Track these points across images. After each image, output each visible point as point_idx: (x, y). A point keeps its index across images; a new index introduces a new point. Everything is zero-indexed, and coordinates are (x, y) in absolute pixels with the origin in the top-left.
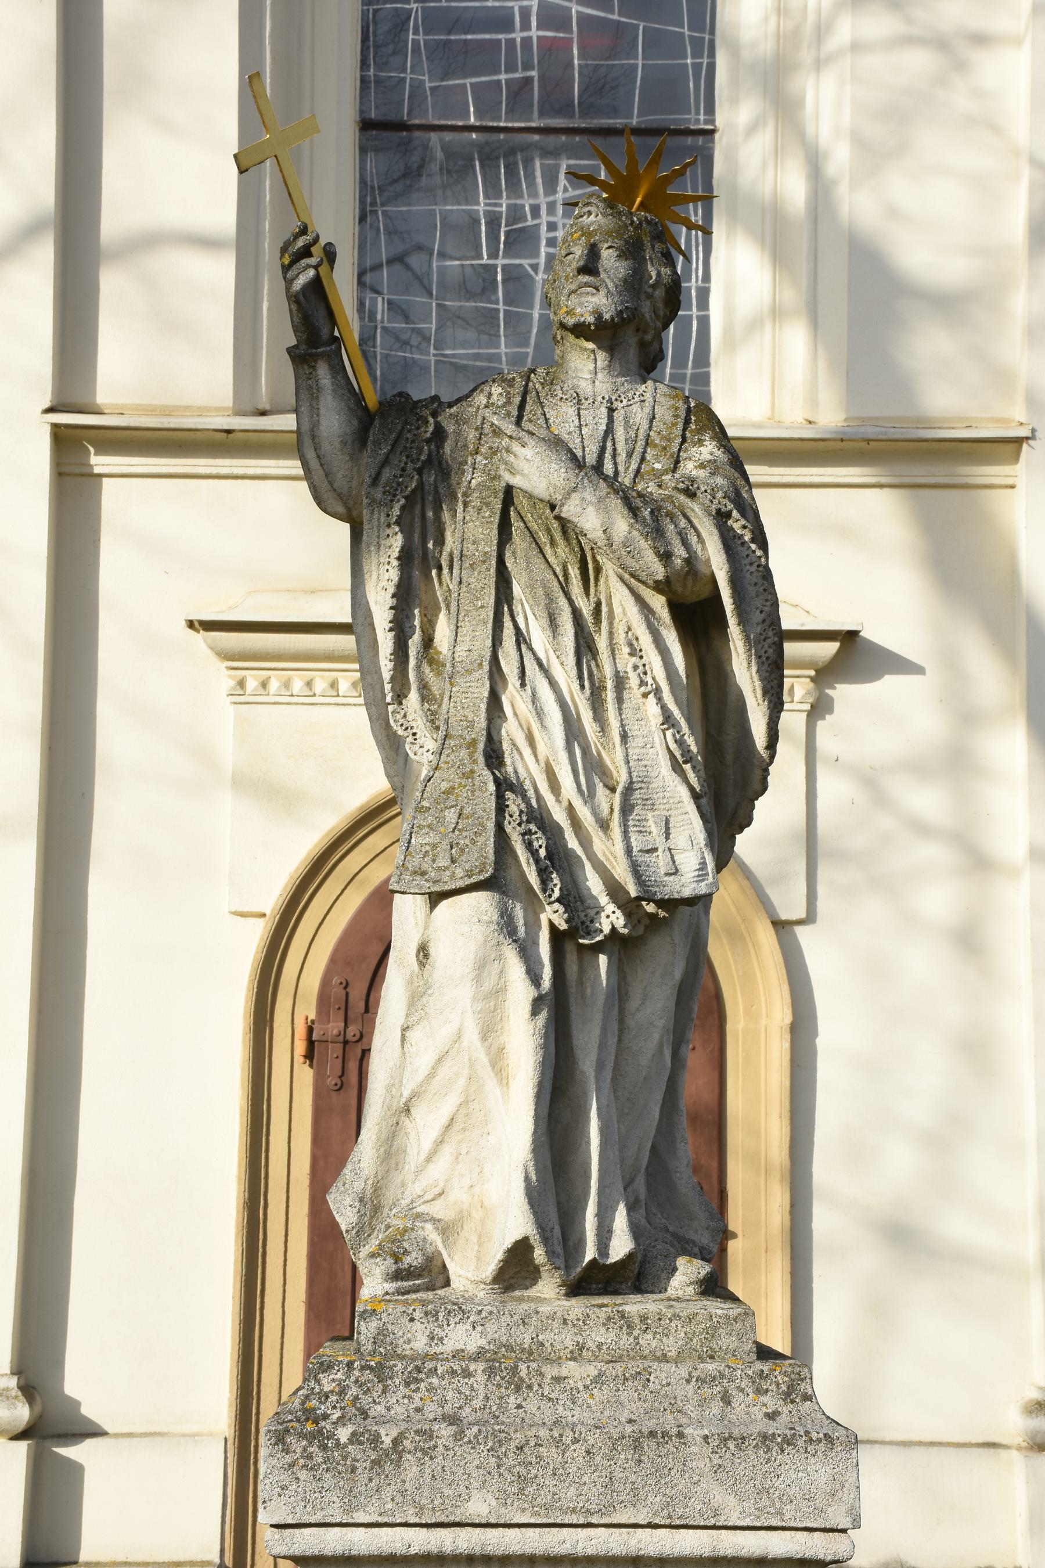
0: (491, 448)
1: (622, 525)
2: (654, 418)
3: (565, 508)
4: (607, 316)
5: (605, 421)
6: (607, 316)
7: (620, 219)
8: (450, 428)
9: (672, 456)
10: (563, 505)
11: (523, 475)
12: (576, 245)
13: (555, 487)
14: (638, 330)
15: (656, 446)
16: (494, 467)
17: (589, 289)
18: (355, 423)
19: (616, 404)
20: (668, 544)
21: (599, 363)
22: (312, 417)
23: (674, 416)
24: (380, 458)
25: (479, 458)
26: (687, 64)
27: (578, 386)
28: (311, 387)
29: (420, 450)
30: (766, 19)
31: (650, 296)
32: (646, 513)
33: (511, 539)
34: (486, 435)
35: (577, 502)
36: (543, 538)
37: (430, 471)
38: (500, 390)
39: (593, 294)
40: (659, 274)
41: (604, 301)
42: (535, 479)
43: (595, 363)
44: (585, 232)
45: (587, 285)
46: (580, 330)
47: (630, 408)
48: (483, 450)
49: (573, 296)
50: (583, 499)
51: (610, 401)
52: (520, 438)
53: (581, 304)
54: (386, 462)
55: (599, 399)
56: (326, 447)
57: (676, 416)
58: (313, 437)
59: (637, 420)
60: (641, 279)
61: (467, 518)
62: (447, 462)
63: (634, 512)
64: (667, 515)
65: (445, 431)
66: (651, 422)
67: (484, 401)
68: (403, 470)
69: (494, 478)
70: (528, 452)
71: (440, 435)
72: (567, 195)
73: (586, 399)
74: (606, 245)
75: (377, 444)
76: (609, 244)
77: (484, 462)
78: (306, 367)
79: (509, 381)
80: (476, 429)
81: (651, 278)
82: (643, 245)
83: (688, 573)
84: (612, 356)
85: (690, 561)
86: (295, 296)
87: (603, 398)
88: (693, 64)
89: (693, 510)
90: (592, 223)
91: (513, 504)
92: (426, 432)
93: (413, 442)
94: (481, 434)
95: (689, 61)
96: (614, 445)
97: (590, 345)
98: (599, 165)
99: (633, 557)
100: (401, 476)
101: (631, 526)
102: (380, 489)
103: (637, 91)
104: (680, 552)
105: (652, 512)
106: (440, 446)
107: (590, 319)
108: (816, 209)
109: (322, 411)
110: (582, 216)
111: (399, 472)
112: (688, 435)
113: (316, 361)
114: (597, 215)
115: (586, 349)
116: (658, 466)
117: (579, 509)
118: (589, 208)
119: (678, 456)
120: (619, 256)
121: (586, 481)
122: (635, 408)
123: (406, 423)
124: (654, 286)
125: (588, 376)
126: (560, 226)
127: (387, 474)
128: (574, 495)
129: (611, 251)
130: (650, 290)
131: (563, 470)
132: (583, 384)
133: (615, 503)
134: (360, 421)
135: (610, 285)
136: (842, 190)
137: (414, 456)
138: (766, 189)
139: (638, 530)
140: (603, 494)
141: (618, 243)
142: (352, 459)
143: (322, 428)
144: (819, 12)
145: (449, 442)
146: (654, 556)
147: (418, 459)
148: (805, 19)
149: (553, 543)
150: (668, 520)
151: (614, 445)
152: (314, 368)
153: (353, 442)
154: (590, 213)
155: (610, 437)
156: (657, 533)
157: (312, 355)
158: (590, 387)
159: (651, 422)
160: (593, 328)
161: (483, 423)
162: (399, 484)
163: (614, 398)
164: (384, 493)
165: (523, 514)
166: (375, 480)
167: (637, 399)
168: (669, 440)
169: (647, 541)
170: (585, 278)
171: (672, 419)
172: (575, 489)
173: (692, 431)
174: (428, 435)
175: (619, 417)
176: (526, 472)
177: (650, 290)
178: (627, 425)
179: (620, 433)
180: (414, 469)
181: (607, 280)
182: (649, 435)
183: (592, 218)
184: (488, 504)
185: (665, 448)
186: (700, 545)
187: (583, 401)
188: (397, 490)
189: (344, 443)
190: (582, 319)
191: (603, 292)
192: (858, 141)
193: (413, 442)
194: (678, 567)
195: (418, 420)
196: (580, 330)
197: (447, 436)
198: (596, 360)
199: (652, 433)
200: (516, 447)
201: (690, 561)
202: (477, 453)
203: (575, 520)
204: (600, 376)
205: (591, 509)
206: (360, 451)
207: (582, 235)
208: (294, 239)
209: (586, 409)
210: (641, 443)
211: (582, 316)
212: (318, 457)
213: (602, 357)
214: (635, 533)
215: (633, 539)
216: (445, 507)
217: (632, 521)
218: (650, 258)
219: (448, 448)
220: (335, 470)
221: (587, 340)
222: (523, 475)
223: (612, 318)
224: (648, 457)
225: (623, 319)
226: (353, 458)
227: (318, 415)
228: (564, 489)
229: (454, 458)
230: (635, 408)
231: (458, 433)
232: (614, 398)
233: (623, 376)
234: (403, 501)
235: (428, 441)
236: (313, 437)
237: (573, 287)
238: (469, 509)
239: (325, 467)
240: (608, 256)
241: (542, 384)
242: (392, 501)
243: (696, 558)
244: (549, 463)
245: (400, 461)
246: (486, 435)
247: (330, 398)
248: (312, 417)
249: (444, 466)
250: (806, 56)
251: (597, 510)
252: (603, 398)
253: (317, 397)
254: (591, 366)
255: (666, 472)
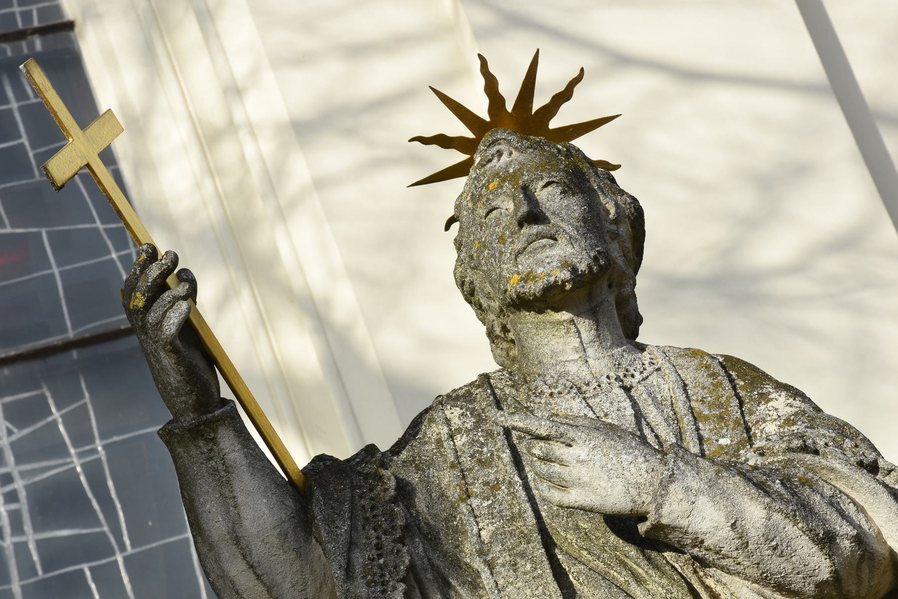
0: (486, 484)
1: (755, 512)
2: (685, 385)
3: (665, 510)
4: (582, 267)
5: (627, 404)
6: (582, 267)
7: (543, 150)
8: (414, 478)
9: (737, 423)
10: (659, 507)
11: (582, 485)
12: (498, 196)
13: (638, 486)
14: (610, 286)
15: (706, 418)
16: (505, 505)
17: (544, 241)
18: (290, 502)
19: (628, 382)
20: (825, 522)
21: (584, 335)
22: (228, 512)
23: (709, 375)
24: (343, 539)
25: (475, 502)
26: (112, 260)
27: (567, 373)
28: (216, 470)
29: (392, 517)
30: (198, 185)
31: (615, 236)
32: (777, 486)
33: (574, 592)
34: (470, 470)
35: (680, 496)
36: (622, 577)
37: (412, 539)
38: (458, 411)
39: (551, 246)
40: (617, 205)
41: (569, 250)
42: (603, 484)
43: (580, 337)
44: (504, 177)
45: (539, 236)
46: (549, 299)
47: (648, 381)
48: (476, 489)
49: (521, 258)
50: (687, 489)
51: (618, 379)
52: (562, 435)
53: (540, 263)
54: (351, 545)
55: (604, 379)
56: (258, 550)
57: (714, 375)
58: (237, 540)
59: (666, 393)
60: (598, 215)
61: (501, 582)
62: (428, 524)
63: (762, 487)
64: (803, 484)
65: (408, 484)
66: (685, 391)
67: (445, 430)
68: (379, 547)
69: (513, 518)
70: (580, 451)
71: (404, 491)
72: (13, 438)
73: (588, 385)
74: (541, 183)
75: (330, 522)
76: (546, 180)
77: (486, 504)
78: (201, 443)
79: (464, 396)
80: (453, 466)
81: (608, 212)
82: (583, 174)
83: (862, 559)
84: (597, 322)
85: (860, 539)
86: (172, 343)
87: (608, 377)
88: (120, 258)
89: (832, 470)
90: (508, 165)
91: (555, 545)
92: (386, 490)
93: (373, 508)
94: (462, 471)
95: (114, 255)
96: (652, 431)
97: (565, 316)
98: (43, 398)
99: (781, 556)
100: (380, 556)
101: (768, 507)
102: (360, 581)
103: (63, 302)
104: (844, 529)
105: (783, 484)
106: (409, 504)
107: (566, 275)
108: (335, 363)
109: (241, 499)
110: (490, 161)
111: (374, 552)
112: (742, 393)
113: (215, 431)
114: (511, 154)
115: (560, 323)
116: (724, 442)
117: (686, 506)
118: (497, 148)
119: (745, 423)
120: (564, 192)
121: (681, 464)
122: (654, 379)
123: (353, 488)
124: (616, 221)
125: (576, 356)
126: (16, 475)
127: (359, 559)
128: (672, 487)
129: (550, 188)
130: (613, 227)
131: (641, 460)
132: (573, 368)
133: (732, 482)
134: (296, 501)
135: (569, 229)
136: (361, 332)
137: (385, 526)
138: (265, 359)
139: (780, 511)
140: (711, 473)
141: (557, 176)
142: (299, 555)
143: (246, 523)
144: (262, 159)
145: (420, 495)
146: (811, 544)
147: (394, 528)
148: (247, 171)
149: (639, 580)
150: (808, 491)
151: (652, 431)
152: (214, 441)
153: (295, 530)
154: (500, 154)
155: (644, 423)
156: (803, 510)
157: (207, 423)
158: (584, 368)
159: (685, 391)
160: (568, 286)
161: (457, 457)
162: (381, 567)
163: (621, 375)
164: (368, 584)
165: (575, 555)
166: (348, 571)
167: (650, 369)
168: (720, 406)
169: (796, 524)
170: (535, 229)
171: (710, 380)
172: (672, 478)
173: (742, 388)
174: (392, 492)
175: (639, 393)
176: (585, 479)
177: (613, 227)
178: (658, 404)
179: (652, 414)
180: (395, 541)
181: (562, 224)
182: (691, 408)
183: (505, 158)
184: (522, 555)
185: (721, 418)
186: (861, 515)
187: (584, 388)
188: (382, 576)
189: (283, 536)
190: (552, 279)
191: (562, 240)
192: (357, 275)
193: (373, 508)
194: (847, 553)
195: (366, 479)
196: (549, 299)
197: (413, 490)
198: (578, 332)
199: (693, 404)
200: (558, 450)
201: (860, 539)
202: (469, 497)
203: (683, 523)
204: (591, 352)
205: (703, 500)
206: (307, 541)
207: (504, 181)
208: (142, 271)
209: (594, 396)
210: (687, 422)
211: (549, 275)
212: (251, 566)
213: (585, 326)
214: (777, 517)
215: (776, 526)
216: (454, 582)
217: (768, 500)
218: (599, 187)
219: (421, 504)
220: (279, 579)
221: (557, 310)
222: (582, 485)
223: (590, 267)
224: (705, 434)
225: (600, 266)
226: (301, 553)
227: (236, 507)
228: (651, 485)
229: (435, 516)
230: (654, 379)
231: (426, 481)
232: (621, 375)
233: (618, 346)
234: (402, 587)
235: (394, 500)
236: (237, 540)
237: (518, 246)
238: (498, 569)
239: (264, 578)
240: (548, 196)
241: (512, 386)
242: (384, 592)
243: (864, 533)
244: (618, 455)
245: (368, 538)
246: (470, 470)
247: (246, 477)
248: (228, 512)
249: (425, 529)
250: (262, 207)
251: (713, 499)
252: (608, 377)
253: (229, 482)
254: (576, 342)
255: (741, 445)
